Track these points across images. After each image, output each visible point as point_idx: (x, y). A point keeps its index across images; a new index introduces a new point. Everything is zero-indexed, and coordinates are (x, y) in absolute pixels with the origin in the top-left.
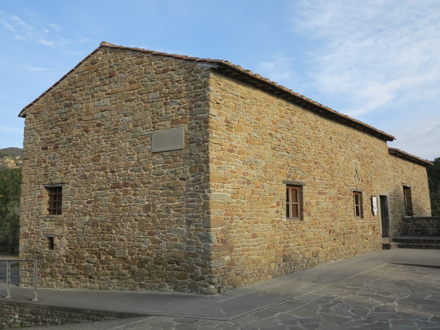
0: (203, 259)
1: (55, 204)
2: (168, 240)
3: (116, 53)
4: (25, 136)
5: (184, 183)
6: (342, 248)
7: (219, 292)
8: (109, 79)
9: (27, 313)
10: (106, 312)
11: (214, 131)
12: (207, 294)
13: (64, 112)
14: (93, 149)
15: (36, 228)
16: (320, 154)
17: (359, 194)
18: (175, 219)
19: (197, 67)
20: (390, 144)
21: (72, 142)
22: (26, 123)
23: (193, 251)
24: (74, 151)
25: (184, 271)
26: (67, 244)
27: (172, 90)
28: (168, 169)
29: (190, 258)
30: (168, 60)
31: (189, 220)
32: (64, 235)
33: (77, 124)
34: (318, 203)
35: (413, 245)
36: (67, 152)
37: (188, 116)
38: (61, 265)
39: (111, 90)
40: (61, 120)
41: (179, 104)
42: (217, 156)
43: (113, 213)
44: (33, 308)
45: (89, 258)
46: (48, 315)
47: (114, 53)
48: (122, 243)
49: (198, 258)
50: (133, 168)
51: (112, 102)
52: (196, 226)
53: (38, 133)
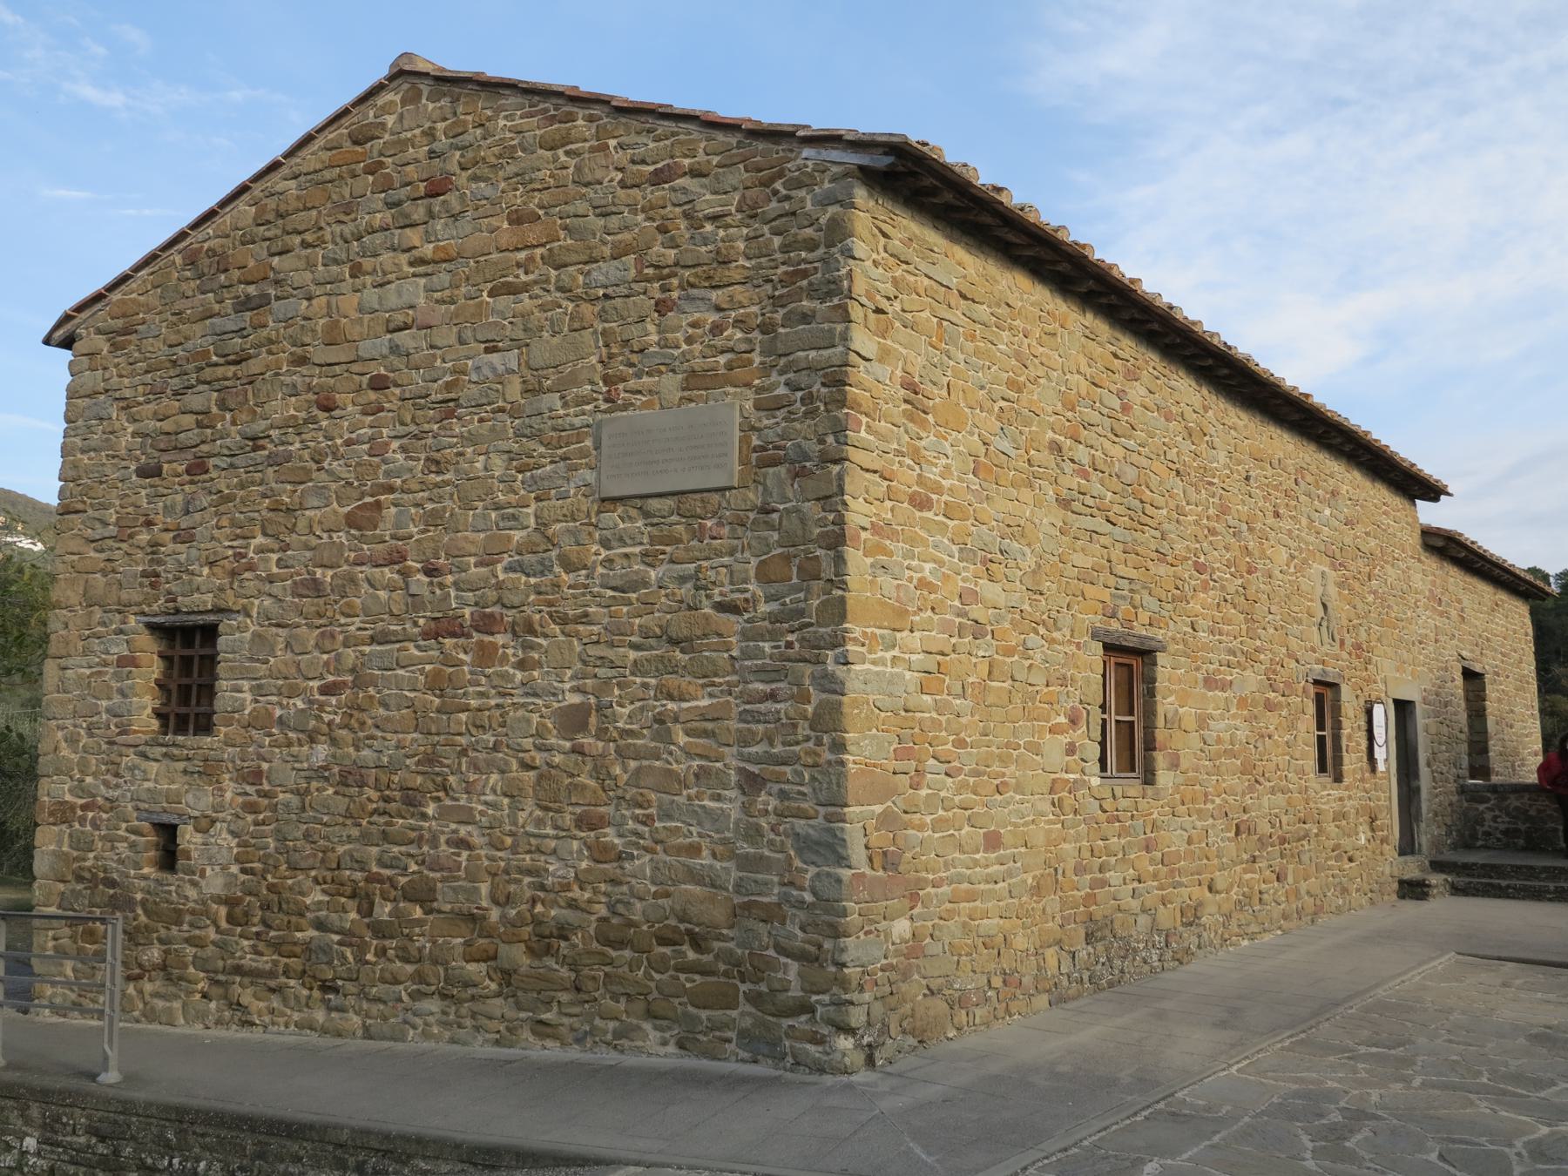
0: (809, 929)
1: (185, 691)
2: (659, 848)
3: (458, 100)
4: (68, 420)
5: (733, 624)
6: (1277, 891)
7: (870, 1061)
8: (425, 201)
9: (74, 1133)
10: (420, 1141)
11: (864, 419)
12: (822, 1071)
13: (235, 328)
14: (351, 477)
15: (106, 784)
16: (1213, 535)
17: (1329, 694)
18: (690, 767)
19: (799, 162)
20: (1429, 513)
21: (264, 448)
22: (76, 369)
23: (766, 895)
24: (274, 485)
25: (726, 974)
26: (235, 851)
27: (691, 251)
28: (665, 567)
29: (751, 923)
30: (677, 134)
31: (753, 773)
32: (220, 815)
33: (288, 380)
34: (1203, 722)
35: (1508, 887)
36: (242, 486)
37: (757, 359)
38: (207, 936)
39: (431, 246)
40: (222, 360)
41: (719, 309)
42: (874, 519)
43: (431, 734)
44: (100, 1114)
45: (324, 913)
46: (168, 1145)
47: (448, 99)
48: (465, 854)
49: (789, 927)
50: (517, 558)
51: (437, 295)
52: (783, 795)
53: (123, 408)
